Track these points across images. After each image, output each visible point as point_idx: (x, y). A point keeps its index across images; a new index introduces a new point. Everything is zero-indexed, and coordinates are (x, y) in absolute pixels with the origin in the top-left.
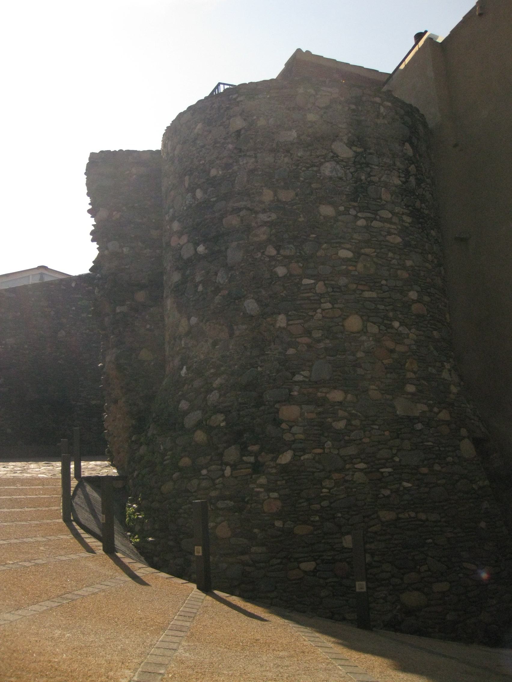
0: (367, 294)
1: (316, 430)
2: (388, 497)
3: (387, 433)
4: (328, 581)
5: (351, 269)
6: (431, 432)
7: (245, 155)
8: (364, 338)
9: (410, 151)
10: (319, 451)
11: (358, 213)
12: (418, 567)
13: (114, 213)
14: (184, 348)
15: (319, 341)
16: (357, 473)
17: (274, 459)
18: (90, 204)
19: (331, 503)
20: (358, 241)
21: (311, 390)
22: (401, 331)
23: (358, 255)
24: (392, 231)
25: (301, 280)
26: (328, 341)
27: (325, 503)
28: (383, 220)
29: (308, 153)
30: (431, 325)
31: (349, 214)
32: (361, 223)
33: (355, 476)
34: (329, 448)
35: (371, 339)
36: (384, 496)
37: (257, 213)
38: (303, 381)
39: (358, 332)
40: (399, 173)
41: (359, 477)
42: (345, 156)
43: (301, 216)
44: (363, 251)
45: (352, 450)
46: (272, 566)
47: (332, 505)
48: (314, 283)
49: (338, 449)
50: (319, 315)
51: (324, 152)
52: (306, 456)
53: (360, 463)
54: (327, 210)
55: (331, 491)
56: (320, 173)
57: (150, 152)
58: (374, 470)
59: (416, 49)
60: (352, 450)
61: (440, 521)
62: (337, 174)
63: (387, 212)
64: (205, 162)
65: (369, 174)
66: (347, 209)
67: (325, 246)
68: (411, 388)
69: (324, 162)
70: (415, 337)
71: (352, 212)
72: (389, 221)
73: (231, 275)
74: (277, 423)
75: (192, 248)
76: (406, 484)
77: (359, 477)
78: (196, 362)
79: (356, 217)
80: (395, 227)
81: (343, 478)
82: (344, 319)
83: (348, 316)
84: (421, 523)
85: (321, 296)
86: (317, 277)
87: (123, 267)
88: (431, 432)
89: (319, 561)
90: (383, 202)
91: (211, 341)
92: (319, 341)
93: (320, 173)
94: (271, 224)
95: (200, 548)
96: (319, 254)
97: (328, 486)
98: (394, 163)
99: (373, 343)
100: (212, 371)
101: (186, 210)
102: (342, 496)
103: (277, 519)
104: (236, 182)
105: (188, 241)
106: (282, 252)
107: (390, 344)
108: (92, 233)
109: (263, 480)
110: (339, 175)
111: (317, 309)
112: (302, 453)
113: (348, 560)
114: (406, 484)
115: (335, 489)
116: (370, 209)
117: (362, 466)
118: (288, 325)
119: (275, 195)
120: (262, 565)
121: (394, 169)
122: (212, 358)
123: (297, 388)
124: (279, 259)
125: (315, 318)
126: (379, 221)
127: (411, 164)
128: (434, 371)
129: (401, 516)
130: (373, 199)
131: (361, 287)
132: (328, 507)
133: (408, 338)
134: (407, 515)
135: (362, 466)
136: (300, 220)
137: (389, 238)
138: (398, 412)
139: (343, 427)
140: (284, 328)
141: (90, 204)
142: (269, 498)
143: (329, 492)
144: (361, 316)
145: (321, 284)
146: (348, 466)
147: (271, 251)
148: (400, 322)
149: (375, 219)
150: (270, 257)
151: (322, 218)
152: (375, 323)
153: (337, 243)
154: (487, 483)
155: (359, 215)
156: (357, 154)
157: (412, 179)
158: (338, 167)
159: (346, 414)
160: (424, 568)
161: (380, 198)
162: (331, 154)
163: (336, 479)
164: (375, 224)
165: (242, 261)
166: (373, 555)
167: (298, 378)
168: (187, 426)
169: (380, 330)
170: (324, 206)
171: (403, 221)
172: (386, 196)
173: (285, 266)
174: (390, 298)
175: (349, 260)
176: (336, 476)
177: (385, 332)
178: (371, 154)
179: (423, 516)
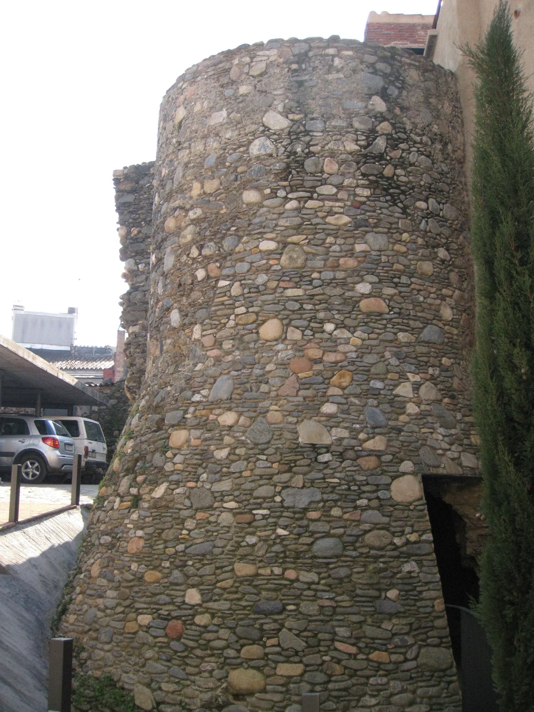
0: (290, 292)
1: (197, 459)
2: (254, 545)
3: (275, 465)
4: (157, 640)
11: (287, 194)
12: (264, 639)
15: (228, 353)
16: (223, 514)
18: (118, 223)
20: (284, 228)
24: (335, 210)
25: (217, 281)
26: (237, 353)
27: (181, 547)
28: (322, 198)
29: (237, 132)
33: (220, 518)
35: (289, 347)
40: (357, 135)
42: (278, 127)
43: (224, 207)
44: (289, 240)
45: (226, 485)
48: (229, 285)
49: (212, 483)
50: (232, 323)
51: (253, 127)
53: (231, 501)
56: (248, 153)
58: (246, 510)
60: (226, 485)
61: (318, 583)
62: (265, 151)
63: (330, 186)
65: (309, 143)
67: (245, 239)
68: (329, 408)
69: (253, 140)
70: (359, 342)
72: (334, 198)
76: (281, 532)
77: (226, 518)
79: (286, 199)
81: (207, 518)
82: (260, 325)
84: (287, 582)
85: (235, 299)
86: (233, 278)
90: (325, 176)
92: (228, 353)
94: (196, 222)
96: (237, 249)
99: (291, 352)
102: (200, 541)
110: (269, 151)
111: (231, 315)
113: (183, 618)
114: (281, 532)
115: (196, 531)
116: (305, 187)
117: (232, 505)
118: (203, 336)
125: (227, 326)
126: (317, 199)
129: (261, 571)
130: (311, 173)
132: (182, 552)
135: (232, 505)
136: (222, 212)
137: (329, 219)
138: (300, 440)
139: (224, 457)
141: (118, 223)
143: (188, 534)
144: (282, 320)
147: (195, 252)
149: (311, 198)
151: (244, 206)
152: (297, 328)
153: (259, 233)
158: (268, 142)
159: (233, 440)
160: (274, 641)
161: (322, 172)
162: (261, 129)
164: (311, 204)
166: (213, 616)
167: (197, 398)
169: (303, 335)
171: (355, 195)
172: (330, 166)
177: (312, 337)
178: (312, 119)
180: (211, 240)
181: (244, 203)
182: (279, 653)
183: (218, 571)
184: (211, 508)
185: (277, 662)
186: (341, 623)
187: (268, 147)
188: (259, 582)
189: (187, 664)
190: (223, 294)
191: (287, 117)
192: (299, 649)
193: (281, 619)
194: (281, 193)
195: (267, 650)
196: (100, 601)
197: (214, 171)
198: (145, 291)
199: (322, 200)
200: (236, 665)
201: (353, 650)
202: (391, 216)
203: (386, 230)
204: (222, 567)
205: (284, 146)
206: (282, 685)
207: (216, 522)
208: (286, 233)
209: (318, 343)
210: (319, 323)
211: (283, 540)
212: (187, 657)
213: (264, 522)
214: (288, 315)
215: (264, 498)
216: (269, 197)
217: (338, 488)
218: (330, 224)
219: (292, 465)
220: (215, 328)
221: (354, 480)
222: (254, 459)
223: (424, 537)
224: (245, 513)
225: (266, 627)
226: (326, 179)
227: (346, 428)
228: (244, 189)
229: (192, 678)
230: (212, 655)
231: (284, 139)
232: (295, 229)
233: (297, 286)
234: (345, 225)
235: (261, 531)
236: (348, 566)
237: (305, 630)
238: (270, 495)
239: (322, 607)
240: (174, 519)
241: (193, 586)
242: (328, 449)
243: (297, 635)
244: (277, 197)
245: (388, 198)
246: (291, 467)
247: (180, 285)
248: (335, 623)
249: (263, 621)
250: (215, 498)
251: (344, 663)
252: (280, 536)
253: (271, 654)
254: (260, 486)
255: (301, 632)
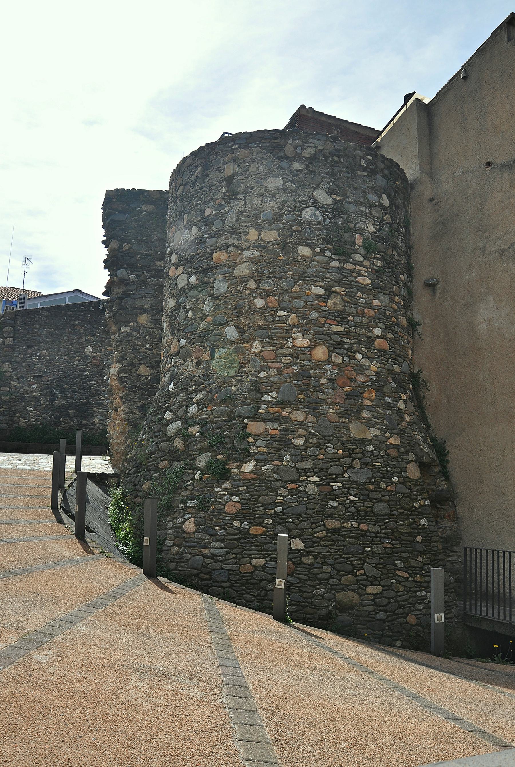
0: (334, 328)
1: (277, 444)
2: (336, 508)
3: (340, 452)
5: (322, 304)
6: (381, 454)
7: (236, 198)
8: (328, 366)
9: (386, 202)
10: (278, 463)
13: (124, 245)
14: (173, 366)
17: (239, 467)
19: (284, 509)
21: (276, 410)
22: (363, 363)
23: (329, 293)
24: (363, 273)
25: (276, 312)
27: (279, 509)
30: (392, 360)
31: (324, 255)
32: (335, 264)
34: (287, 461)
36: (332, 507)
37: (242, 250)
38: (271, 401)
39: (324, 361)
40: (374, 220)
41: (312, 489)
45: (307, 465)
46: (228, 559)
47: (284, 511)
51: (306, 198)
52: (266, 467)
54: (304, 251)
55: (285, 499)
57: (160, 192)
59: (405, 108)
60: (307, 465)
61: (380, 533)
64: (202, 202)
66: (323, 251)
69: (306, 208)
71: (328, 253)
73: (216, 304)
74: (245, 436)
75: (186, 279)
78: (181, 379)
80: (366, 270)
81: (297, 488)
83: (316, 346)
86: (291, 311)
87: (129, 292)
88: (381, 454)
89: (268, 559)
91: (195, 361)
93: (301, 217)
94: (253, 261)
95: (148, 538)
96: (294, 289)
97: (282, 494)
98: (371, 212)
100: (194, 387)
101: (183, 244)
103: (236, 520)
104: (226, 221)
105: (183, 273)
106: (262, 286)
107: (353, 374)
108: (105, 262)
109: (227, 485)
112: (263, 464)
117: (315, 479)
118: (262, 351)
119: (260, 234)
120: (219, 558)
121: (369, 217)
122: (195, 376)
123: (264, 406)
124: (258, 291)
127: (386, 214)
128: (390, 400)
131: (329, 321)
132: (281, 512)
133: (369, 369)
134: (350, 525)
135: (315, 479)
137: (359, 279)
140: (258, 353)
141: (104, 236)
142: (231, 500)
143: (283, 500)
144: (328, 347)
145: (294, 315)
146: (302, 478)
147: (252, 284)
148: (363, 355)
150: (251, 289)
152: (339, 354)
154: (428, 502)
155: (333, 257)
156: (336, 202)
157: (386, 228)
158: (318, 213)
160: (362, 572)
162: (312, 201)
163: (291, 489)
165: (227, 292)
166: (315, 558)
167: (266, 398)
168: (169, 433)
169: (343, 360)
170: (302, 247)
171: (374, 265)
173: (263, 298)
174: (356, 332)
175: (320, 296)
176: (290, 486)
177: (348, 362)
179: (364, 527)
180: (269, 278)
181: (298, 255)
182: (366, 580)
183: (313, 526)
184: (298, 481)
185: (366, 586)
186: (397, 558)
187: (318, 216)
188: (345, 533)
189: (303, 592)
190: (282, 322)
191: (331, 197)
192: (378, 576)
193: (364, 557)
194: (328, 253)
195: (358, 578)
196: (205, 551)
197: (270, 223)
198: (135, 299)
199: (355, 264)
200: (339, 589)
201: (407, 575)
202: (390, 283)
203: (388, 293)
204: (315, 523)
205: (329, 218)
206: (372, 600)
207: (305, 491)
208: (332, 283)
209: (353, 367)
210: (353, 353)
211: (355, 504)
212: (302, 586)
213: (340, 492)
214: (333, 345)
215: (337, 475)
216: (318, 254)
217: (381, 469)
218: (359, 283)
219: (351, 452)
220: (275, 346)
221: (389, 465)
222: (325, 447)
223: (426, 503)
224: (325, 485)
225: (354, 563)
226: (357, 249)
227: (378, 429)
228: (299, 244)
229: (309, 600)
230: (321, 584)
231: (330, 213)
232: (337, 282)
233: (339, 324)
234: (368, 285)
235: (338, 498)
236: (395, 521)
237: (379, 564)
238: (341, 473)
239: (385, 548)
240: (268, 488)
241: (296, 537)
242: (370, 442)
243: (375, 567)
244: (324, 255)
245: (390, 270)
246: (351, 454)
247: (236, 308)
248: (395, 558)
249: (352, 559)
250: (300, 473)
251: (403, 583)
252: (353, 501)
253: (361, 580)
254: (331, 466)
255: (377, 565)
